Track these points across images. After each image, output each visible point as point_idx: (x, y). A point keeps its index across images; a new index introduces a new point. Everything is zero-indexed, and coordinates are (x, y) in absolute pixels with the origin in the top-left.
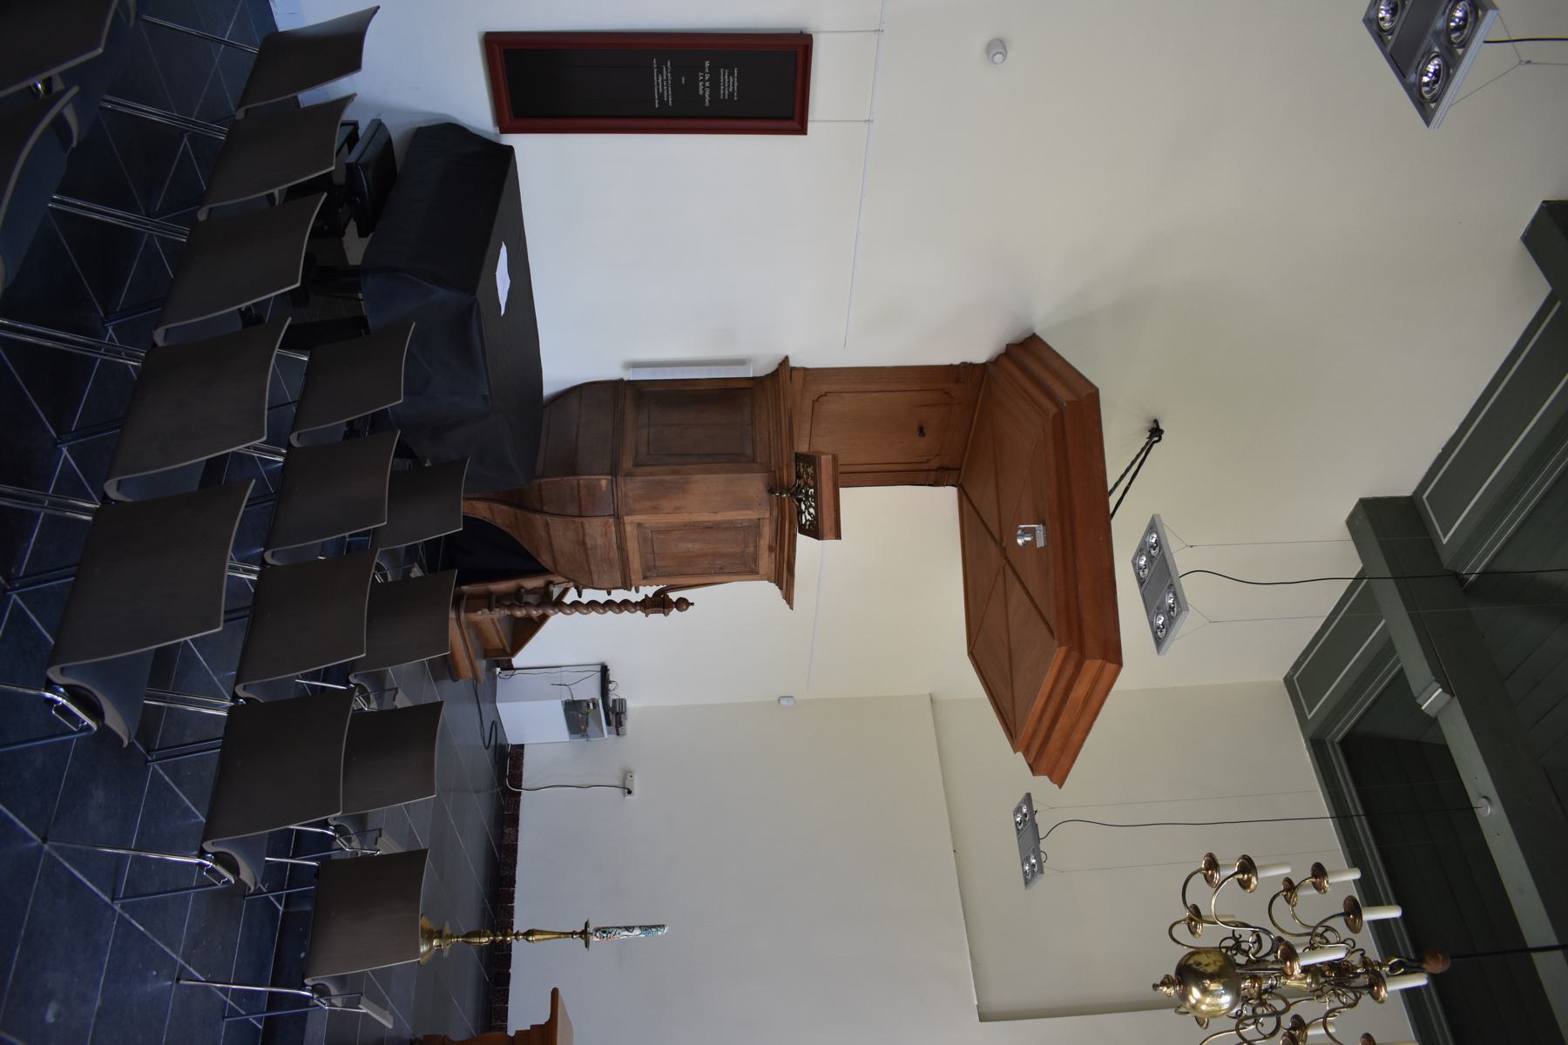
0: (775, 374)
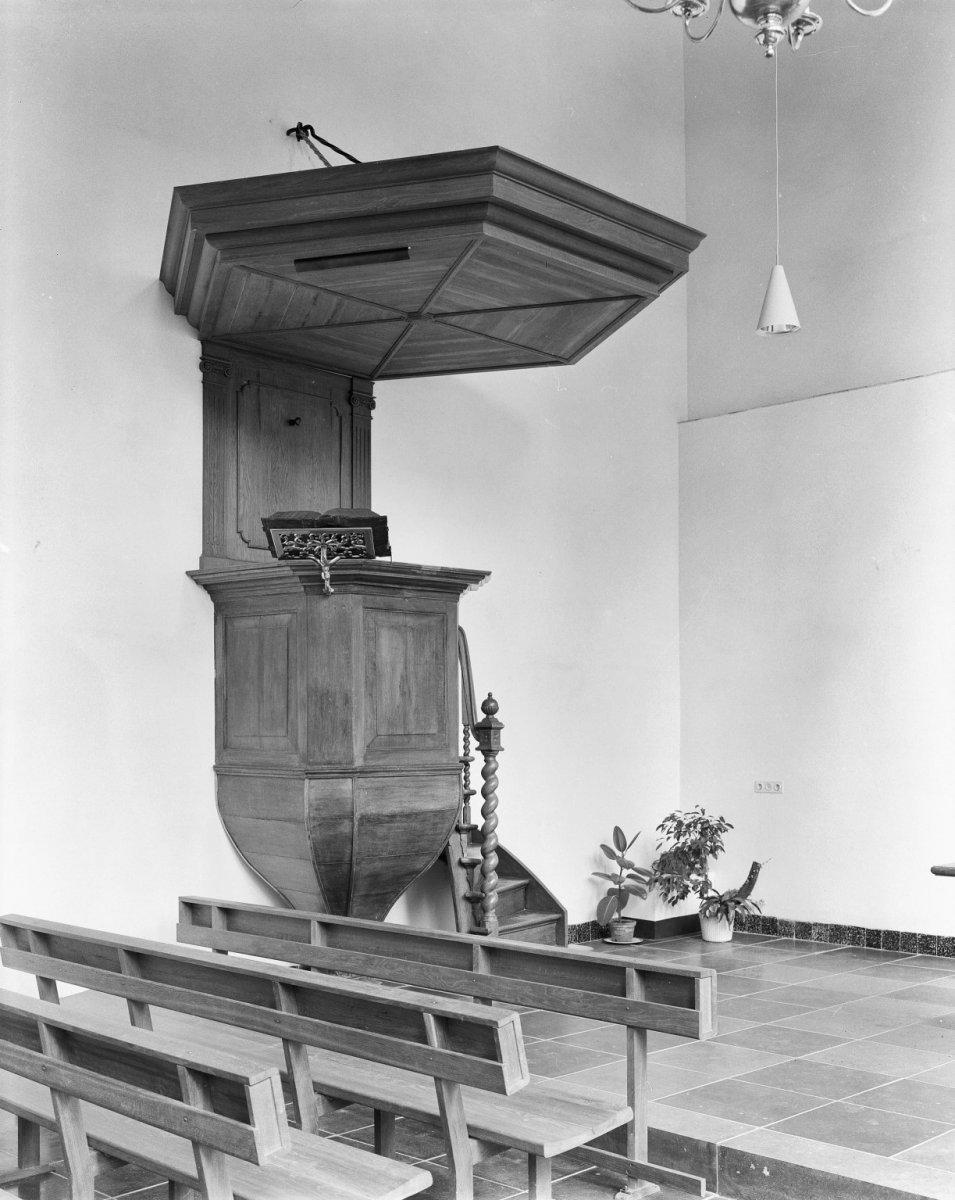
0: (210, 589)
